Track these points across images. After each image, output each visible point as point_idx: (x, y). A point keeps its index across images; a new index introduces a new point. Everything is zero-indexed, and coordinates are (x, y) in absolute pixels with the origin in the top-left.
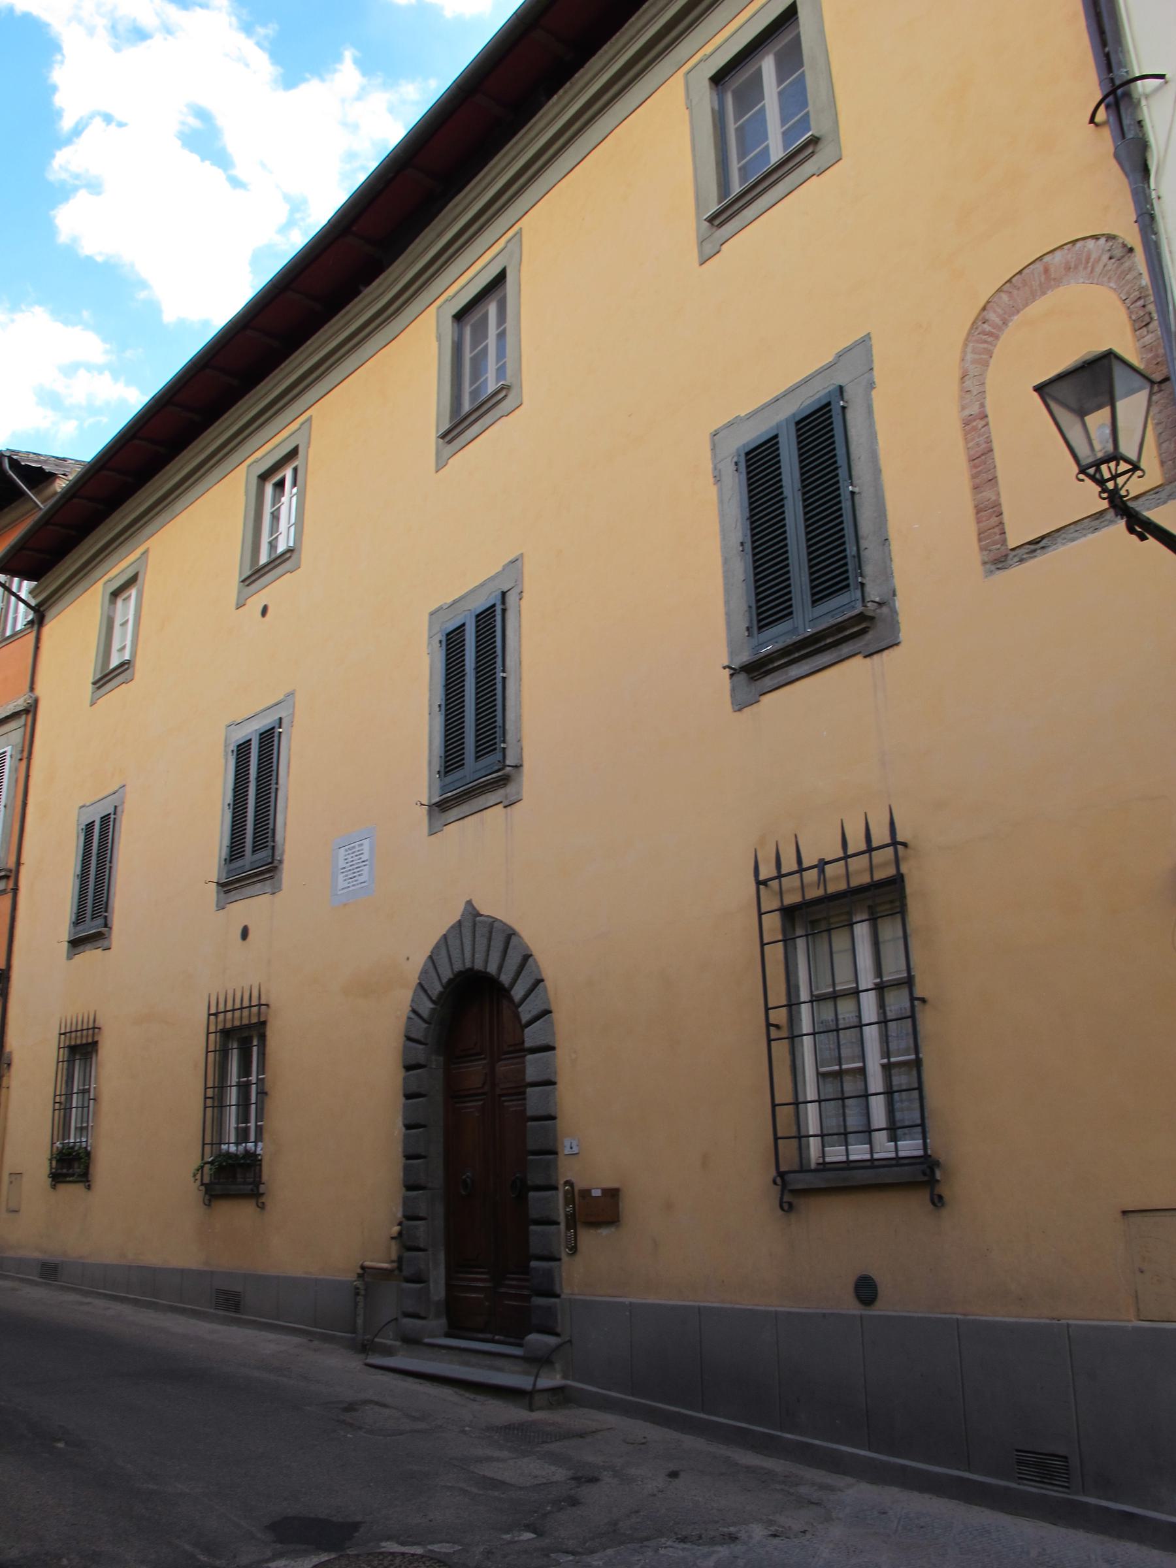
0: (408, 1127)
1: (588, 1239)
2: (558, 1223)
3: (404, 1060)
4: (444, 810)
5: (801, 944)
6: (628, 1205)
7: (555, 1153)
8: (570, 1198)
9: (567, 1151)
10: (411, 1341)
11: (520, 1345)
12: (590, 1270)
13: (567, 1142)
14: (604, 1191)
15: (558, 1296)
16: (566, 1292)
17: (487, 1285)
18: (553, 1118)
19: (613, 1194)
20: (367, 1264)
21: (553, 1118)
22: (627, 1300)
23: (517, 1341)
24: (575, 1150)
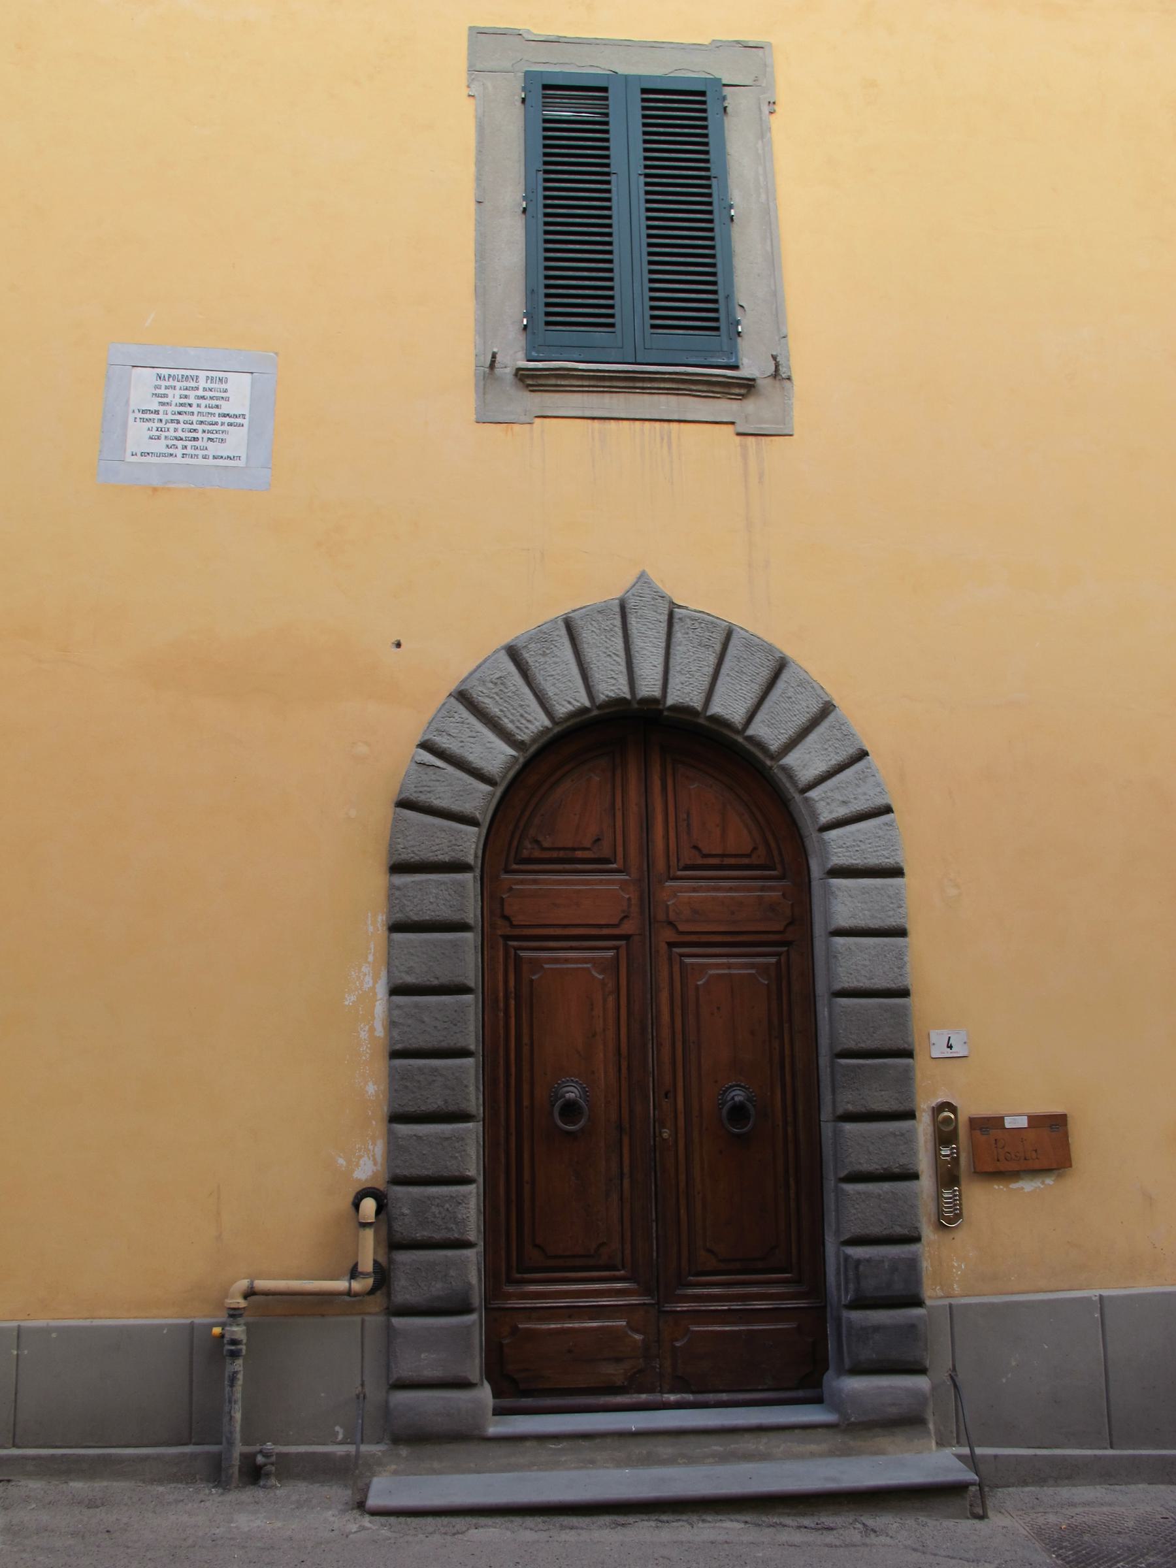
0: (396, 990)
1: (983, 1201)
2: (915, 1176)
3: (392, 849)
4: (533, 389)
5: (669, 771)
6: (1080, 1138)
7: (909, 1054)
8: (945, 1136)
9: (939, 1050)
10: (418, 1439)
11: (818, 1400)
12: (987, 1255)
13: (938, 1039)
14: (1036, 1121)
15: (918, 1302)
16: (931, 1292)
17: (634, 1300)
18: (904, 993)
19: (1054, 1126)
20: (262, 1284)
21: (904, 993)
22: (1093, 1293)
23: (809, 1393)
24: (959, 1050)
